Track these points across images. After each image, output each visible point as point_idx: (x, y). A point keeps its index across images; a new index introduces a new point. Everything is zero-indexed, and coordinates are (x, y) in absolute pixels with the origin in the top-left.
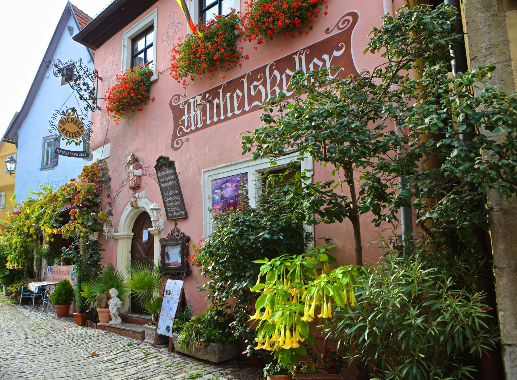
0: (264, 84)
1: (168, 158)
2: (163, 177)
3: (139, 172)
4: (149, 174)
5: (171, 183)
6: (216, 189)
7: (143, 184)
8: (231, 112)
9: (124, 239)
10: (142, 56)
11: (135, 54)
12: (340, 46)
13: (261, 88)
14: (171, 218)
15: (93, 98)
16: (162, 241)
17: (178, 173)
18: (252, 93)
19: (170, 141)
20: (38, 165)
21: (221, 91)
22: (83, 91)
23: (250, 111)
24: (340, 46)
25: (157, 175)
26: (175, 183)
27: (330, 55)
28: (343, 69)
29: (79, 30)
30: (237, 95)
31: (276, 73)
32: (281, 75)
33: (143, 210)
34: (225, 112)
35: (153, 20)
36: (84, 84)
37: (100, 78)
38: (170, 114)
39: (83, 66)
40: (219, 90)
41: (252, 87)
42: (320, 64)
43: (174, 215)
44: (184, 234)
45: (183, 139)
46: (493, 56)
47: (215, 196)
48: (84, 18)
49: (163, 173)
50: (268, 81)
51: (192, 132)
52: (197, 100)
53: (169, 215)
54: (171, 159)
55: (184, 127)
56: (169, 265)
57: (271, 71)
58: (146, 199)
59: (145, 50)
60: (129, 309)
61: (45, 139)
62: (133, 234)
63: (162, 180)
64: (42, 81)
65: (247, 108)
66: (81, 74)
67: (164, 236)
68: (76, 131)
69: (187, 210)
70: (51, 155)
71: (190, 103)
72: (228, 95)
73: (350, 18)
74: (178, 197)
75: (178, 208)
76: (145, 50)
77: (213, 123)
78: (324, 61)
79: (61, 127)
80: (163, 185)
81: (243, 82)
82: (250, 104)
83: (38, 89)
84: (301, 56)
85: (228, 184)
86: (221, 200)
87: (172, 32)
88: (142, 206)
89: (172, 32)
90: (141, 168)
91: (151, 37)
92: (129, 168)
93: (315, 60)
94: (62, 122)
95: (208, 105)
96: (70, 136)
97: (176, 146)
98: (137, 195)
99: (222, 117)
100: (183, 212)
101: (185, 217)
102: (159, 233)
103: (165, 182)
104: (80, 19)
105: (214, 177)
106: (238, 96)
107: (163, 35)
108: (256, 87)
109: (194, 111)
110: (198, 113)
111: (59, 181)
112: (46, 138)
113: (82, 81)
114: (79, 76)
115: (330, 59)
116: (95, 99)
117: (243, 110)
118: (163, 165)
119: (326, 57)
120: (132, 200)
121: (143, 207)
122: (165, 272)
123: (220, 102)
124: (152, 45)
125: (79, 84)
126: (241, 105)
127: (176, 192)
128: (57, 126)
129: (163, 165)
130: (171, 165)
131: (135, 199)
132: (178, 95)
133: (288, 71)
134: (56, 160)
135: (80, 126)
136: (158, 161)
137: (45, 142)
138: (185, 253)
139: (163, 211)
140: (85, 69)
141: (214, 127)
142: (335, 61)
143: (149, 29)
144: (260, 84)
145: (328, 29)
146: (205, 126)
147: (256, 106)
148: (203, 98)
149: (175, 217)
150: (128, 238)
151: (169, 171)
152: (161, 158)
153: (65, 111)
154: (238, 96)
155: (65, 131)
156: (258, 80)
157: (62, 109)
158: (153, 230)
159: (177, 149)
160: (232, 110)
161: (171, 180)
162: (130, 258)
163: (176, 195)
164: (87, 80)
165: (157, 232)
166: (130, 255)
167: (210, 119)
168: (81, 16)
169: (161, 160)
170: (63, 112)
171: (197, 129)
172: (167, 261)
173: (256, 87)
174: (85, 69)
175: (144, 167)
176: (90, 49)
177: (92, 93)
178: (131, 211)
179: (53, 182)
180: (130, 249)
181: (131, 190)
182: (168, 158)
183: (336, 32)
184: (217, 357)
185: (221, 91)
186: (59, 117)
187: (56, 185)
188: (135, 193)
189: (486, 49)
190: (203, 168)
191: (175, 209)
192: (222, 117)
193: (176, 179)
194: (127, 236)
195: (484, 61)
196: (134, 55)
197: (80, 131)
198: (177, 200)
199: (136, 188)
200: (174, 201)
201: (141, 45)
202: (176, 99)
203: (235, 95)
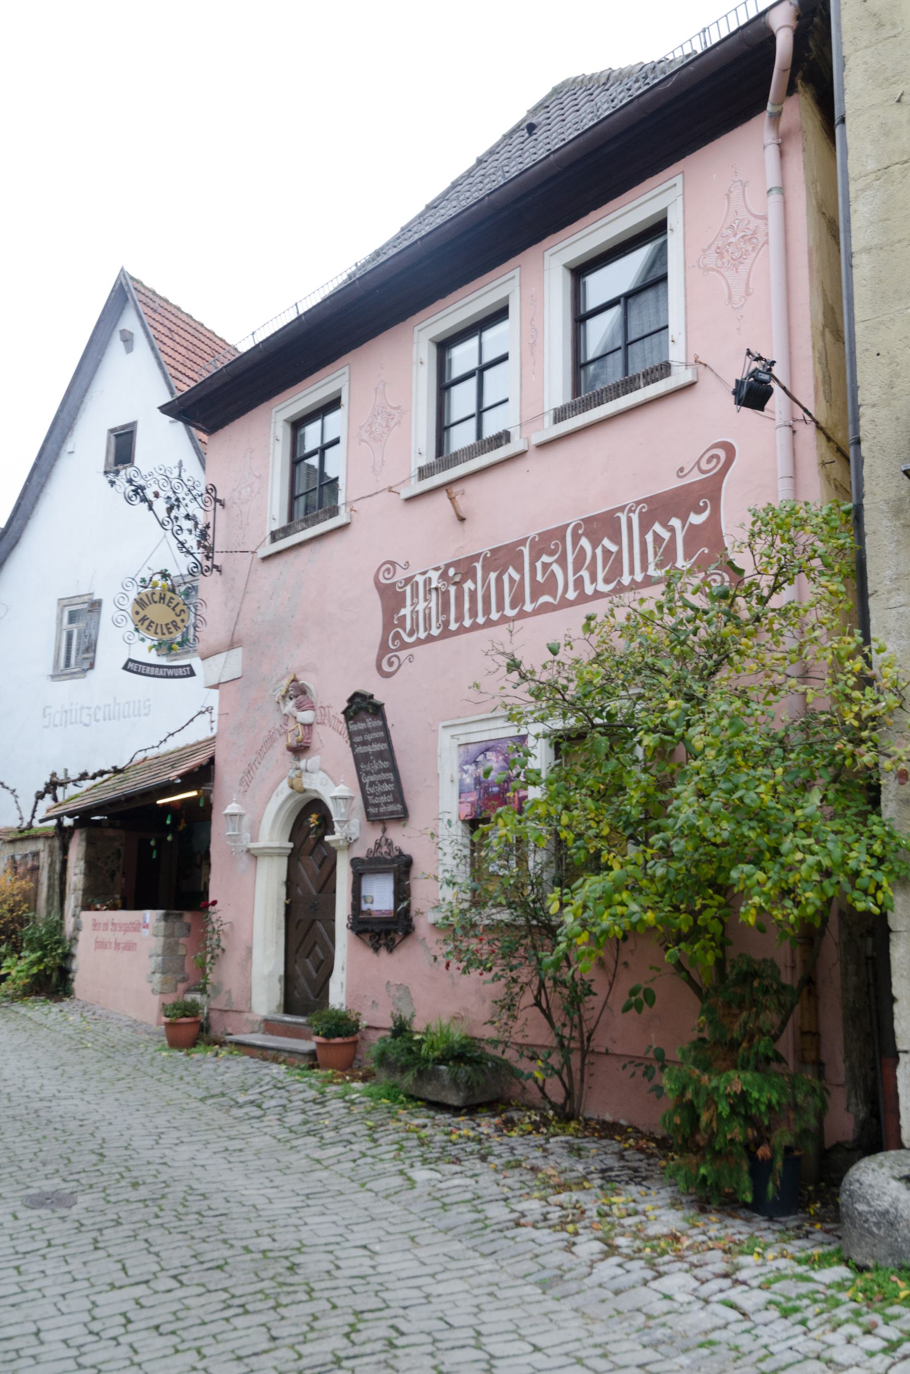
0: (562, 562)
1: (372, 697)
2: (360, 733)
3: (306, 716)
4: (330, 721)
5: (377, 747)
6: (467, 763)
7: (315, 743)
8: (498, 611)
9: (271, 855)
10: (314, 461)
11: (298, 456)
12: (701, 504)
13: (556, 568)
14: (375, 818)
15: (205, 547)
16: (355, 862)
17: (389, 726)
18: (539, 578)
19: (373, 656)
20: (47, 665)
21: (479, 566)
22: (186, 533)
23: (536, 612)
24: (701, 504)
25: (348, 728)
26: (383, 746)
27: (684, 520)
28: (706, 551)
29: (172, 393)
30: (511, 578)
31: (585, 542)
32: (594, 547)
33: (315, 795)
34: (487, 611)
35: (340, 390)
36: (187, 517)
37: (219, 501)
38: (375, 599)
39: (185, 476)
40: (476, 564)
41: (539, 565)
42: (666, 535)
43: (382, 810)
44: (400, 851)
45: (403, 654)
46: (901, 592)
47: (465, 776)
48: (160, 310)
49: (361, 726)
50: (570, 558)
51: (420, 642)
52: (430, 579)
53: (371, 810)
54: (378, 698)
55: (405, 630)
56: (369, 912)
57: (576, 539)
58: (321, 774)
59: (321, 451)
60: (278, 1006)
61: (63, 603)
62: (291, 845)
63: (358, 739)
64: (55, 460)
65: (528, 607)
66: (180, 496)
67: (360, 852)
68: (169, 621)
69: (408, 802)
70: (79, 644)
71: (417, 583)
72: (493, 576)
73: (722, 454)
74: (390, 776)
75: (390, 798)
76: (321, 451)
77: (462, 630)
78: (672, 530)
79: (137, 613)
80: (360, 750)
81: (521, 552)
82: (534, 599)
83: (46, 481)
84: (631, 515)
85: (490, 755)
86: (476, 784)
87: (380, 425)
88: (313, 787)
89: (380, 425)
90: (312, 708)
91: (335, 423)
92: (285, 705)
93: (657, 527)
94: (140, 603)
95: (452, 590)
96: (156, 633)
97: (386, 668)
98: (302, 764)
99: (481, 620)
100: (399, 807)
101: (402, 816)
102: (349, 846)
103: (364, 743)
104: (150, 312)
105: (463, 740)
106: (511, 579)
107: (361, 428)
108: (546, 566)
109: (426, 600)
110: (433, 605)
111: (98, 707)
112: (65, 602)
113: (182, 512)
114: (177, 500)
115: (683, 527)
116: (209, 552)
117: (521, 609)
118: (360, 709)
119: (675, 522)
120: (293, 774)
121: (316, 791)
122: (361, 928)
123: (476, 589)
124: (336, 442)
125: (176, 518)
126: (517, 601)
127: (386, 764)
128: (129, 610)
129: (360, 709)
130: (377, 710)
131: (297, 772)
132: (393, 563)
133: (606, 542)
134: (90, 655)
135: (178, 609)
136: (351, 700)
137: (62, 612)
138: (402, 893)
139: (358, 801)
140: (190, 484)
141: (464, 637)
142: (693, 534)
143: (333, 404)
144: (556, 561)
145: (681, 470)
146: (446, 633)
147: (546, 604)
148: (444, 576)
149: (384, 814)
150: (280, 855)
151: (371, 723)
152: (356, 695)
153: (148, 580)
154: (511, 579)
155: (147, 623)
156: (551, 553)
157: (142, 575)
158: (337, 841)
159: (387, 675)
160: (500, 607)
161: (377, 740)
162: (284, 897)
163: (385, 771)
164: (194, 509)
165: (346, 844)
166: (283, 891)
167: (456, 621)
168: (152, 305)
169: (358, 700)
170: (143, 580)
171: (430, 639)
172: (365, 907)
173: (546, 566)
174: (190, 484)
175: (318, 705)
176: (193, 429)
177: (203, 535)
178: (290, 797)
179: (82, 708)
180: (284, 878)
181: (290, 753)
182: (372, 697)
183: (696, 477)
184: (462, 1094)
185: (479, 566)
186: (133, 594)
187: (89, 715)
188: (299, 760)
189: (891, 580)
190: (443, 720)
191: (383, 799)
192: (481, 620)
193: (387, 739)
194: (278, 851)
195: (888, 600)
196: (297, 460)
197: (178, 619)
198: (388, 782)
199: (299, 750)
200: (382, 782)
201: (312, 436)
202: (388, 570)
203: (506, 578)
